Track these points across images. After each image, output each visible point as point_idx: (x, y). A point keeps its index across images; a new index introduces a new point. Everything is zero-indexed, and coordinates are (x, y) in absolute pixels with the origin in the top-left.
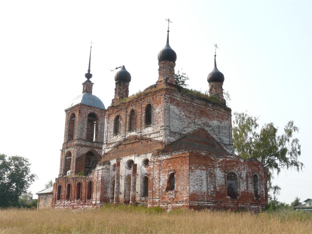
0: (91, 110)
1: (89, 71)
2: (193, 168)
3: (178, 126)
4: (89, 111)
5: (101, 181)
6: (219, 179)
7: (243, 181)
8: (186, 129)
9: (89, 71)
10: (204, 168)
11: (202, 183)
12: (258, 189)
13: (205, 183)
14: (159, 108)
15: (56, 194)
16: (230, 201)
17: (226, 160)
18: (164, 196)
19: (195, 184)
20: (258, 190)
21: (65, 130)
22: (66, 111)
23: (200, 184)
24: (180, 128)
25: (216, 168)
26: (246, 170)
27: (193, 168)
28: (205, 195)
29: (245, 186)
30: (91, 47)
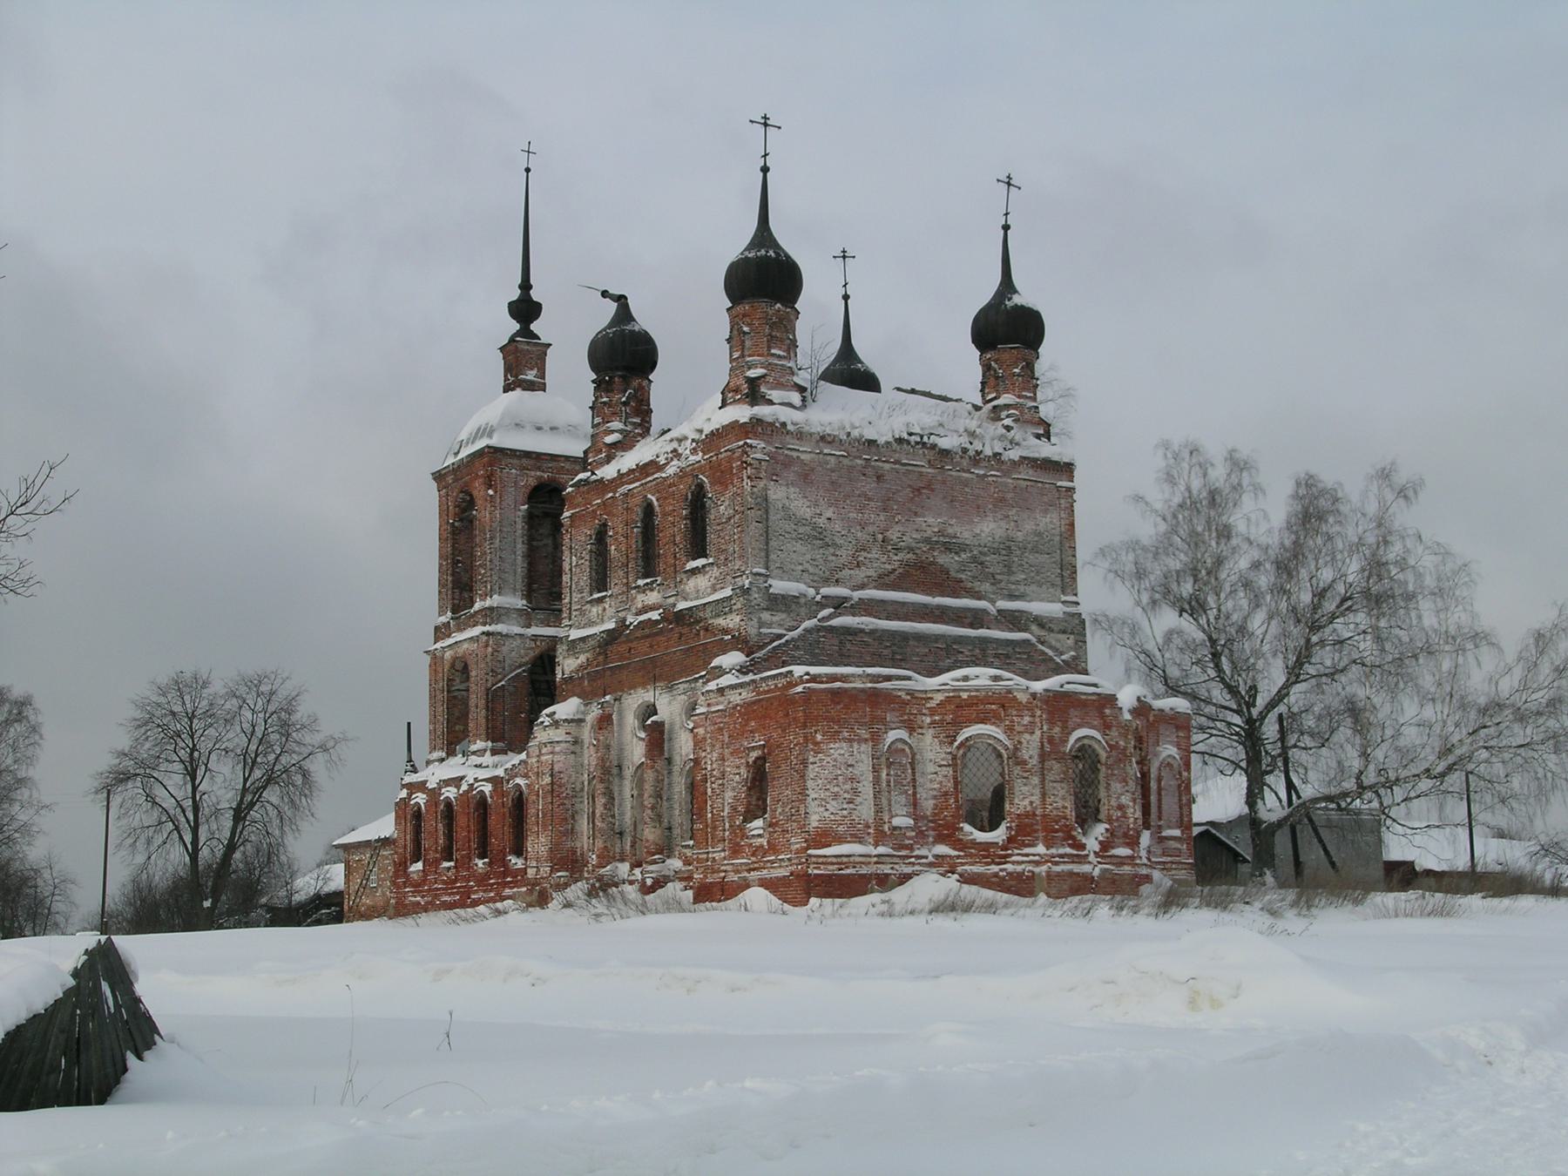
0: (539, 469)
1: (526, 286)
2: (819, 737)
3: (807, 566)
4: (532, 478)
5: (549, 788)
6: (934, 771)
7: (1025, 775)
8: (846, 572)
9: (526, 286)
10: (864, 734)
11: (856, 792)
12: (1099, 801)
13: (867, 789)
14: (727, 503)
15: (405, 845)
16: (973, 851)
17: (960, 697)
18: (738, 840)
19: (827, 794)
20: (1102, 803)
21: (441, 565)
22: (439, 477)
23: (846, 795)
24: (817, 571)
25: (920, 731)
26: (1038, 733)
27: (819, 737)
28: (869, 834)
29: (1037, 791)
30: (528, 170)
